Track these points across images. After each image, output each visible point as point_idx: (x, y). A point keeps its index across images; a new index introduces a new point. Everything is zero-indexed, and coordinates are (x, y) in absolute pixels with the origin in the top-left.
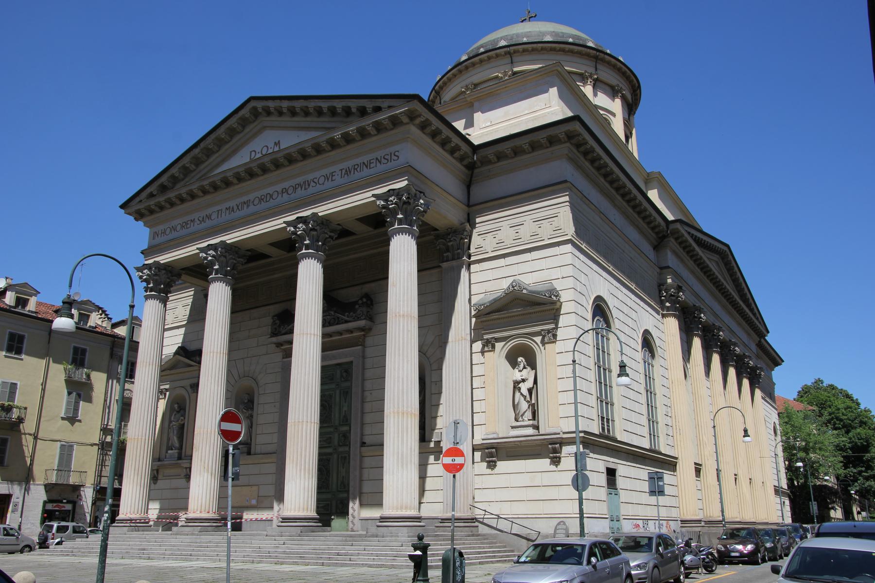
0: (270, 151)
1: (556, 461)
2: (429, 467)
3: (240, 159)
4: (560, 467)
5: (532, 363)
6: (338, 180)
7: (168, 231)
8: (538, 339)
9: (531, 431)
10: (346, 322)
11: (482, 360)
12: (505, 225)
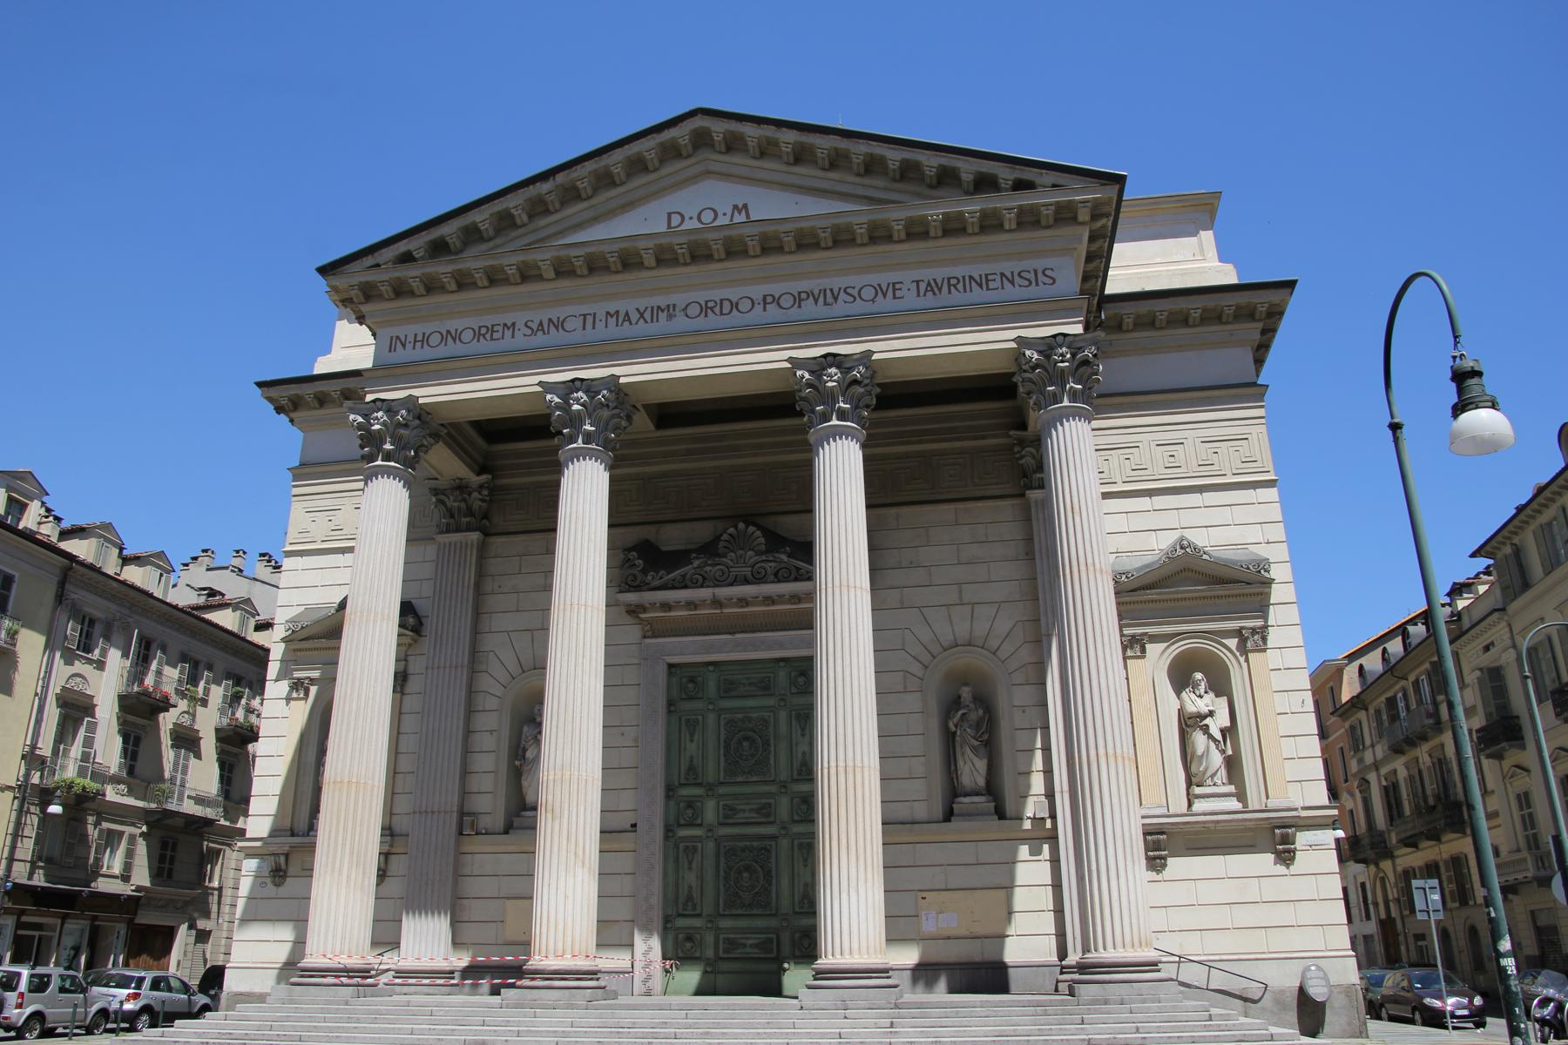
1: (1286, 857)
3: (644, 222)
4: (1294, 869)
5: (1220, 685)
6: (910, 299)
7: (435, 339)
8: (1232, 643)
9: (1234, 804)
12: (1145, 439)
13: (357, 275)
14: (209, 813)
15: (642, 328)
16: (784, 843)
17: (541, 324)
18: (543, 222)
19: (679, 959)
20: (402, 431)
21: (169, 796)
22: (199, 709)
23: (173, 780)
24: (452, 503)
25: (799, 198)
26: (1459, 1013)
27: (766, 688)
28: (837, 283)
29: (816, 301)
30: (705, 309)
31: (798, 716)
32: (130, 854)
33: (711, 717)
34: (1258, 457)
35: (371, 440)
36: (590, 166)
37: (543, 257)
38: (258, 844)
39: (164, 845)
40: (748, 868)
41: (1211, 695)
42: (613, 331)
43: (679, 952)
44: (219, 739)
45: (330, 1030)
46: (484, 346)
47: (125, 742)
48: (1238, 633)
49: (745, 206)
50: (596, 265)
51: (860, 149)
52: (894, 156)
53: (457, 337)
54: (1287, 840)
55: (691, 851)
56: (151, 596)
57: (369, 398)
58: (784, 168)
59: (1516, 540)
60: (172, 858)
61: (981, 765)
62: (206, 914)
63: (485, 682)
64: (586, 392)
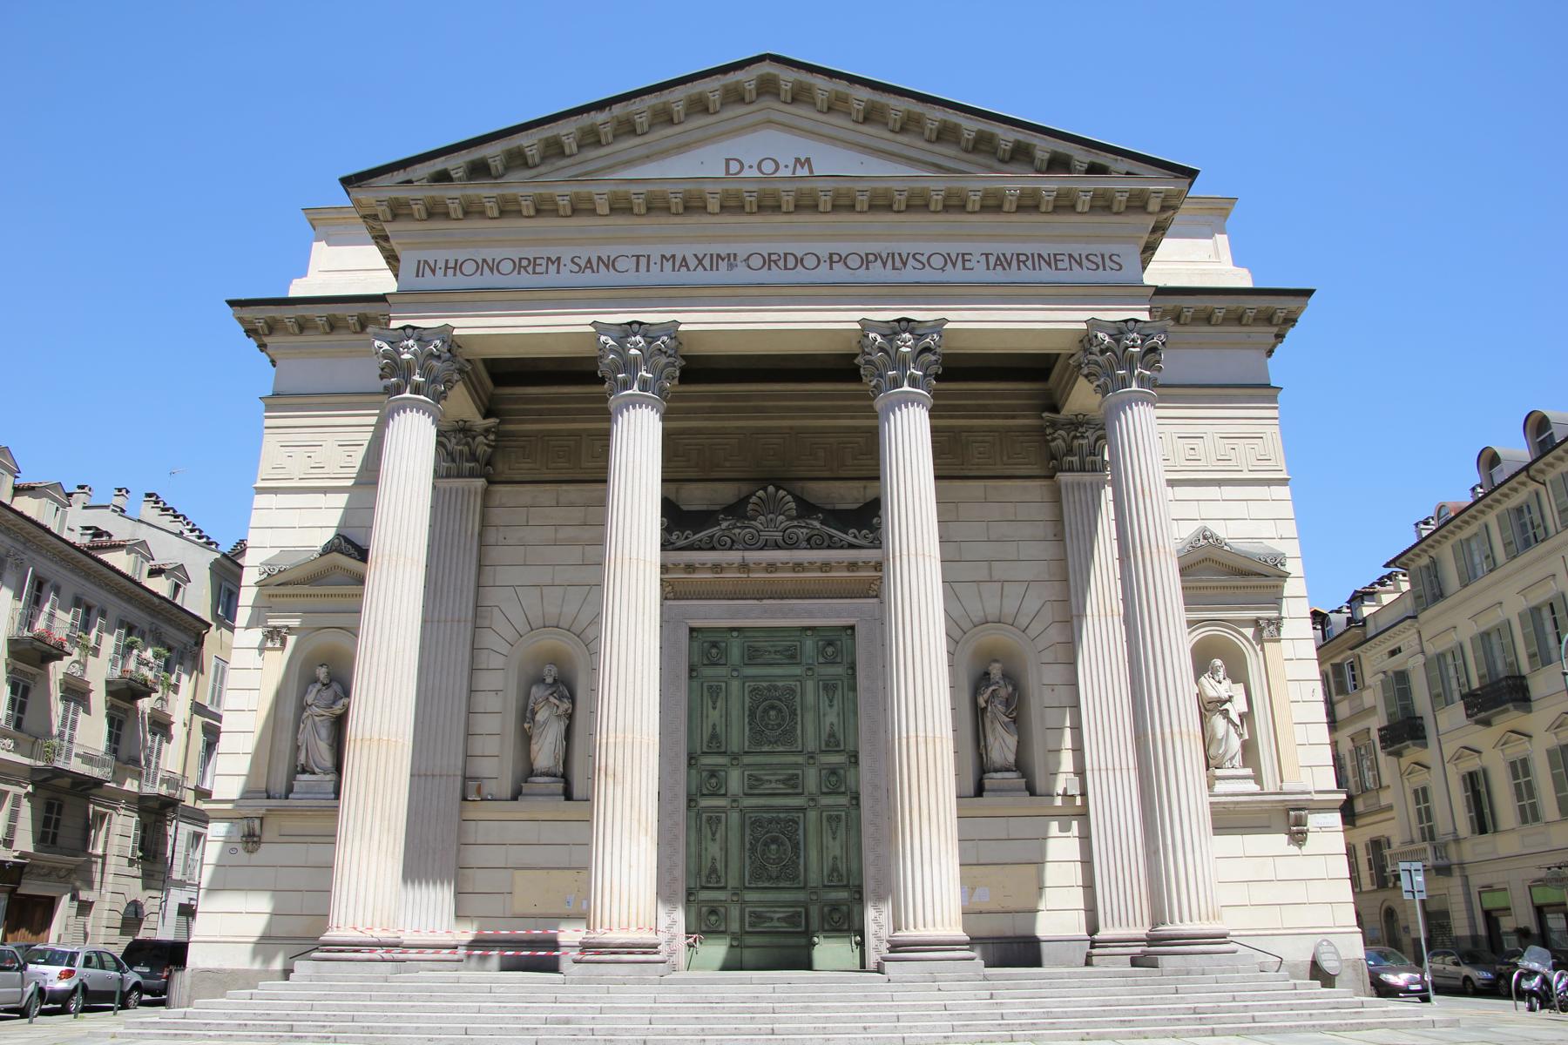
0: (782, 173)
1: (1298, 837)
2: (1051, 844)
3: (699, 164)
5: (1237, 673)
6: (980, 272)
7: (469, 268)
9: (1251, 786)
10: (851, 546)
11: (258, 662)
13: (387, 189)
14: (96, 772)
15: (700, 276)
16: (812, 815)
17: (589, 261)
18: (592, 153)
19: (703, 933)
20: (434, 363)
21: (56, 751)
22: (90, 658)
23: (61, 735)
24: (452, 444)
25: (864, 158)
26: (1413, 987)
27: (793, 657)
28: (906, 248)
29: (884, 264)
30: (768, 261)
31: (826, 688)
32: (14, 816)
33: (735, 685)
34: (1202, 457)
35: (394, 367)
36: (651, 100)
37: (600, 191)
38: (229, 806)
39: (49, 807)
40: (774, 840)
41: (1228, 681)
42: (669, 275)
43: (703, 925)
44: (109, 693)
45: (383, 1009)
46: (525, 279)
47: (14, 691)
48: (1256, 622)
49: (808, 160)
50: (657, 205)
51: (936, 115)
52: (970, 126)
53: (494, 267)
54: (1300, 822)
55: (714, 821)
56: (48, 531)
57: (394, 324)
58: (851, 125)
59: (1433, 553)
60: (57, 821)
61: (1012, 741)
62: (89, 885)
63: (488, 639)
64: (418, 340)
